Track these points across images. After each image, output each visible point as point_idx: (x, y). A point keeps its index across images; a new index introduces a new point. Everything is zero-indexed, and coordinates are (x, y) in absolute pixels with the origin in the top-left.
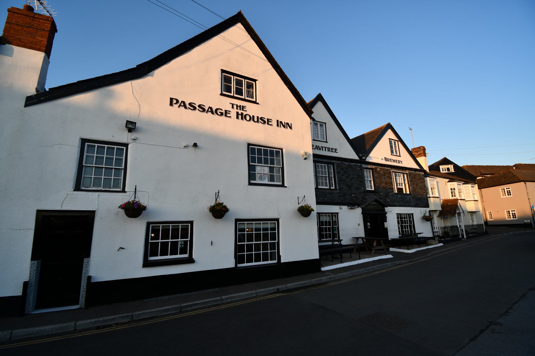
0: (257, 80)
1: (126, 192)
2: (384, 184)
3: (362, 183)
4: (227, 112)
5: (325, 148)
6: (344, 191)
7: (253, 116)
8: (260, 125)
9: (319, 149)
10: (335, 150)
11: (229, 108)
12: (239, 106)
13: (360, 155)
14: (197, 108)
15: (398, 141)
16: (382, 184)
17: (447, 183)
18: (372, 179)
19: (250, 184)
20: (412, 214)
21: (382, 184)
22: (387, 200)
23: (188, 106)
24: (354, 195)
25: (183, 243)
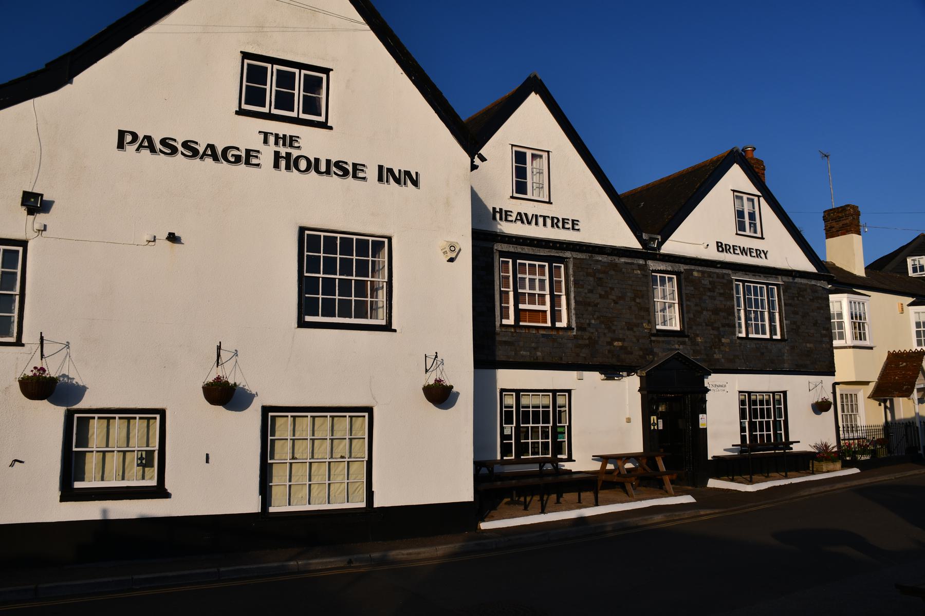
0: (332, 70)
1: (23, 345)
2: (711, 314)
3: (647, 310)
4: (252, 153)
5: (545, 218)
6: (592, 333)
7: (317, 160)
8: (334, 181)
9: (525, 221)
10: (573, 224)
11: (256, 143)
12: (280, 138)
13: (645, 236)
14: (180, 148)
15: (759, 197)
16: (705, 313)
17: (905, 307)
18: (677, 301)
19: (302, 324)
20: (785, 393)
21: (705, 313)
22: (715, 355)
23: (158, 146)
24: (620, 344)
25: (144, 456)
